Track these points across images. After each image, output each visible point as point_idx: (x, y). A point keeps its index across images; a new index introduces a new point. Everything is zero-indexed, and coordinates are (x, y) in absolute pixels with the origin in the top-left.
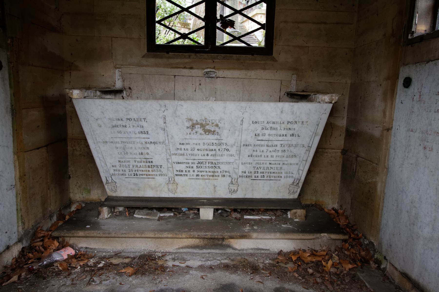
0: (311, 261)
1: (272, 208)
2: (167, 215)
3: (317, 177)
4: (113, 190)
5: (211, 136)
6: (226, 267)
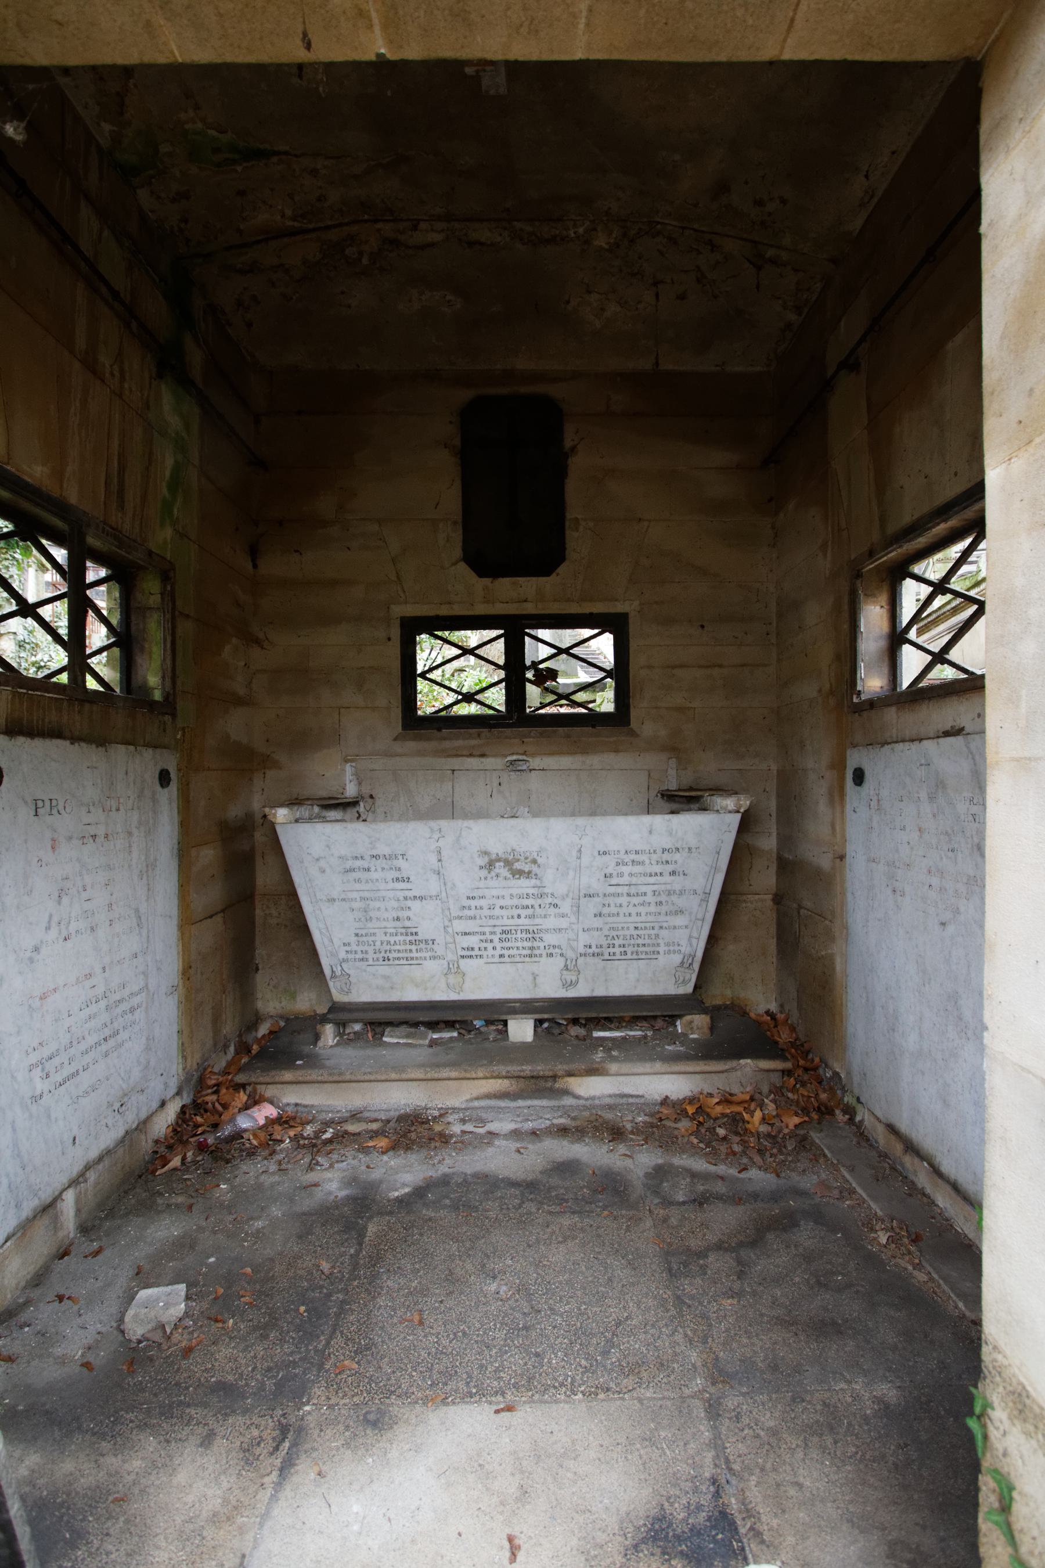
0: (722, 1114)
1: (645, 1014)
2: (446, 1035)
3: (730, 951)
5: (524, 882)
6: (563, 1131)
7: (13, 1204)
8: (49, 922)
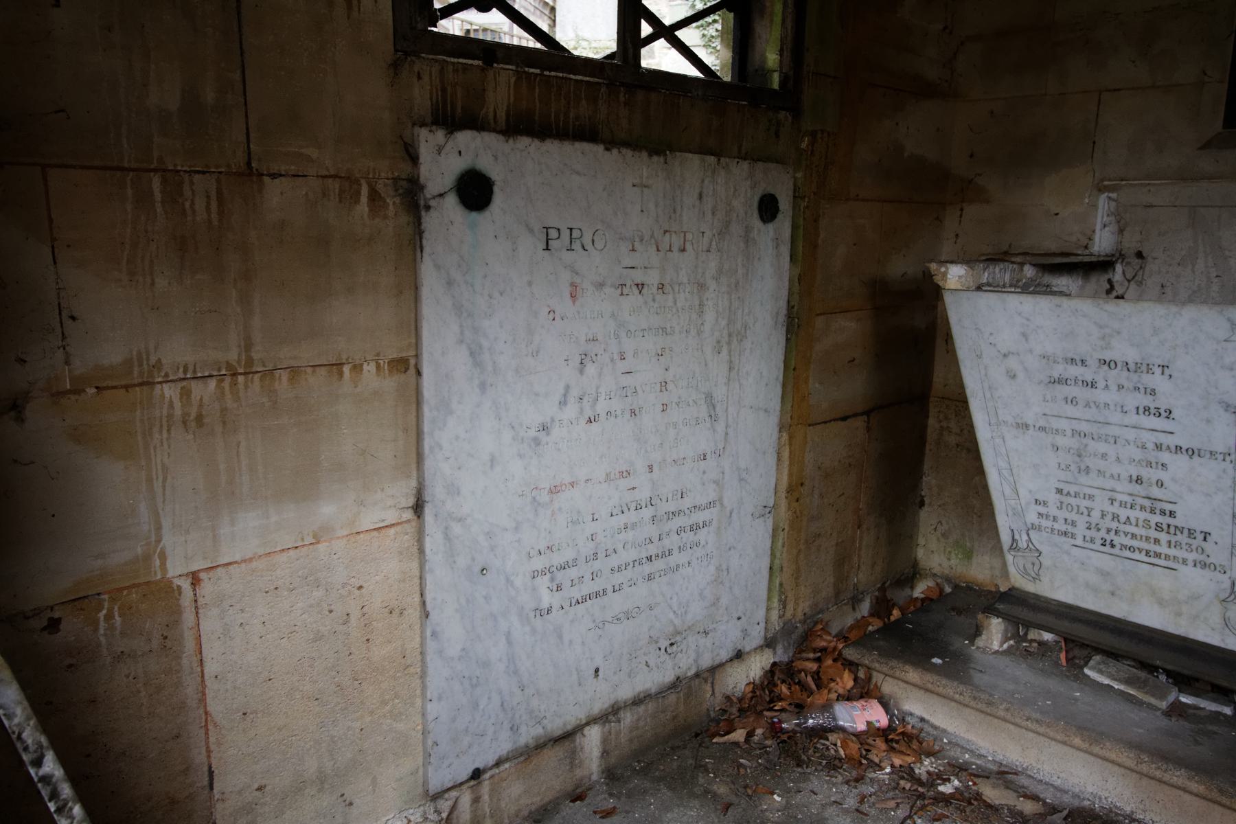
2: (1210, 706)
4: (1028, 574)
7: (507, 726)
8: (565, 395)
